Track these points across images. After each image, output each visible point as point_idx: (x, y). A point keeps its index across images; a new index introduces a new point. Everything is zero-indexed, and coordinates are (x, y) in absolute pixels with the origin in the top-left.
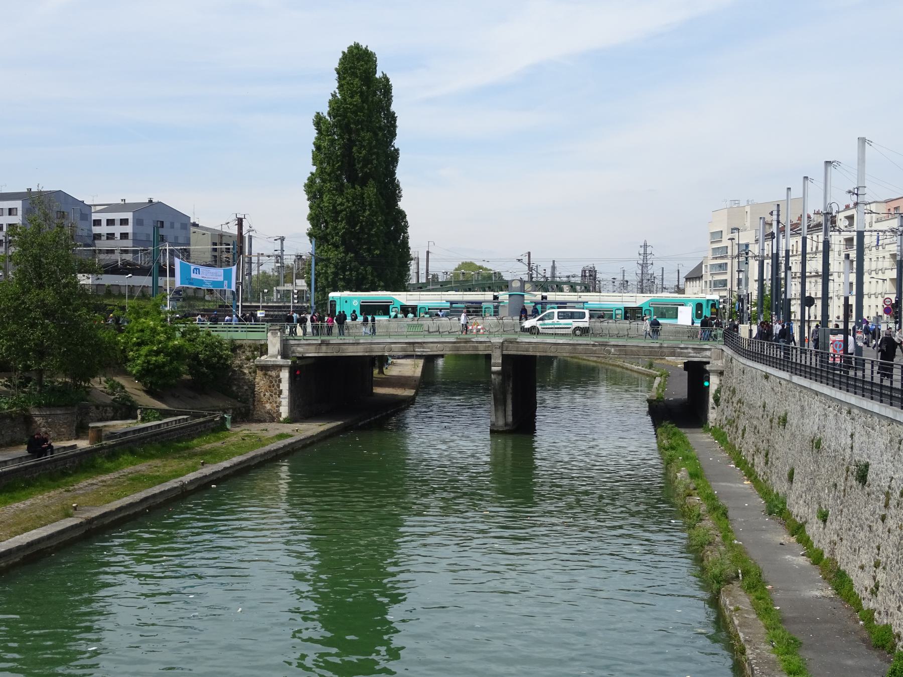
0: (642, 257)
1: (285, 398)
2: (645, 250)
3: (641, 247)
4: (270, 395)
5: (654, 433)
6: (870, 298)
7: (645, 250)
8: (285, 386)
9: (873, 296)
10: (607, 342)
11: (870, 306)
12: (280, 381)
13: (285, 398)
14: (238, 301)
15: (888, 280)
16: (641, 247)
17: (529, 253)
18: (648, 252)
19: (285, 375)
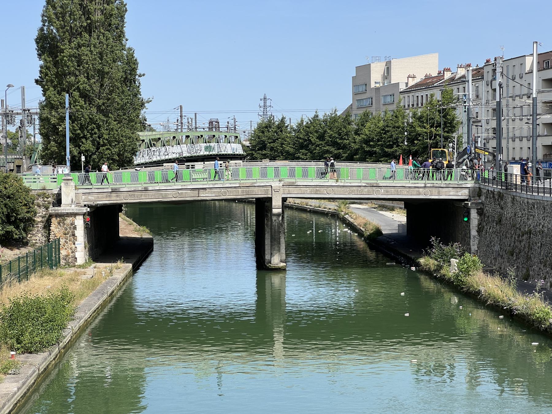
0: (262, 109)
1: (80, 244)
2: (265, 103)
3: (261, 100)
4: (65, 241)
5: (50, 235)
6: (521, 140)
7: (265, 103)
8: (80, 232)
9: (517, 140)
10: (293, 183)
11: (514, 148)
12: (75, 228)
13: (80, 244)
14: (439, 150)
15: (541, 125)
16: (261, 100)
17: (181, 107)
18: (268, 104)
19: (80, 222)
